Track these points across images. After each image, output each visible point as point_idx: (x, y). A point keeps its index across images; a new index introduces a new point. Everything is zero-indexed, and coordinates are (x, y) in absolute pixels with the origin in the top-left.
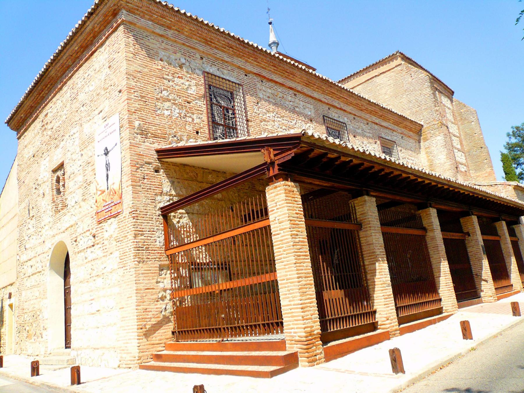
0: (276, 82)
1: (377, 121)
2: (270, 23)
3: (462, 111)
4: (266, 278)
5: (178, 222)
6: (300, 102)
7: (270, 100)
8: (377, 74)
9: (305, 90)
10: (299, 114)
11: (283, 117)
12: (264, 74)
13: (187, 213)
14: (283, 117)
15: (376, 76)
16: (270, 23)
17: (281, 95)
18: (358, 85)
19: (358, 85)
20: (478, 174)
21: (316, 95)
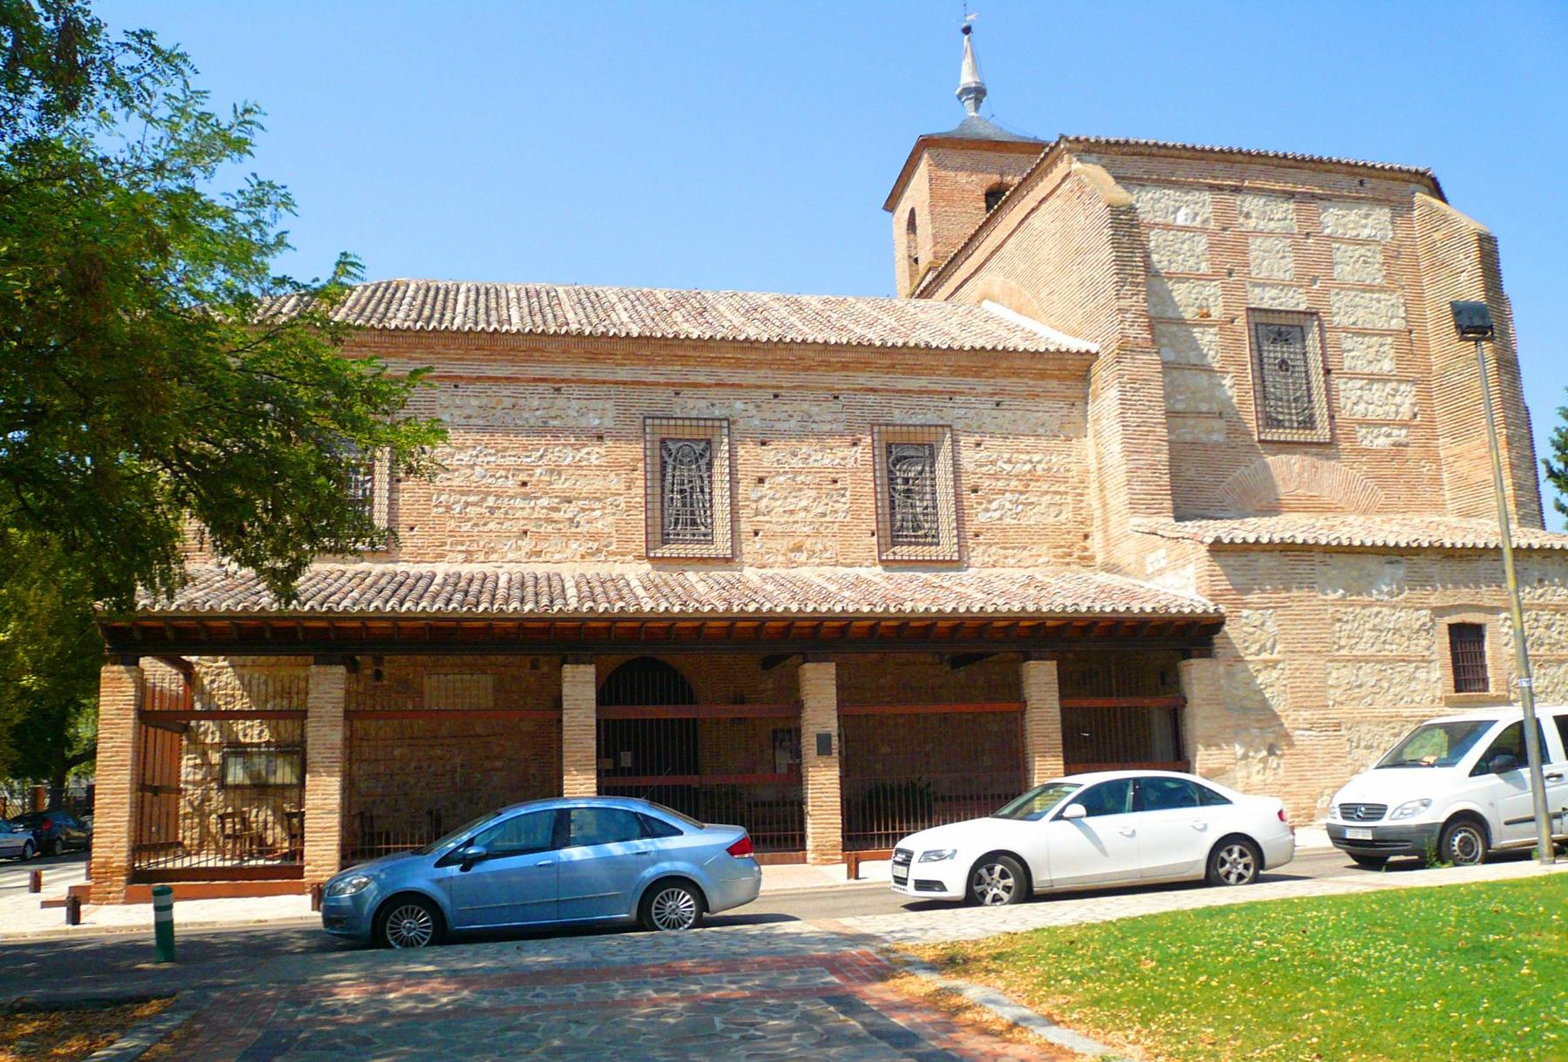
0: (496, 379)
1: (876, 383)
2: (967, 30)
3: (1437, 236)
4: (1071, 703)
5: (212, 682)
6: (570, 406)
7: (472, 421)
8: (1034, 204)
9: (588, 372)
10: (556, 433)
11: (505, 449)
12: (458, 371)
13: (233, 666)
14: (505, 449)
15: (1033, 210)
16: (967, 30)
17: (508, 402)
18: (1010, 235)
19: (1010, 235)
20: (1458, 450)
21: (623, 374)
